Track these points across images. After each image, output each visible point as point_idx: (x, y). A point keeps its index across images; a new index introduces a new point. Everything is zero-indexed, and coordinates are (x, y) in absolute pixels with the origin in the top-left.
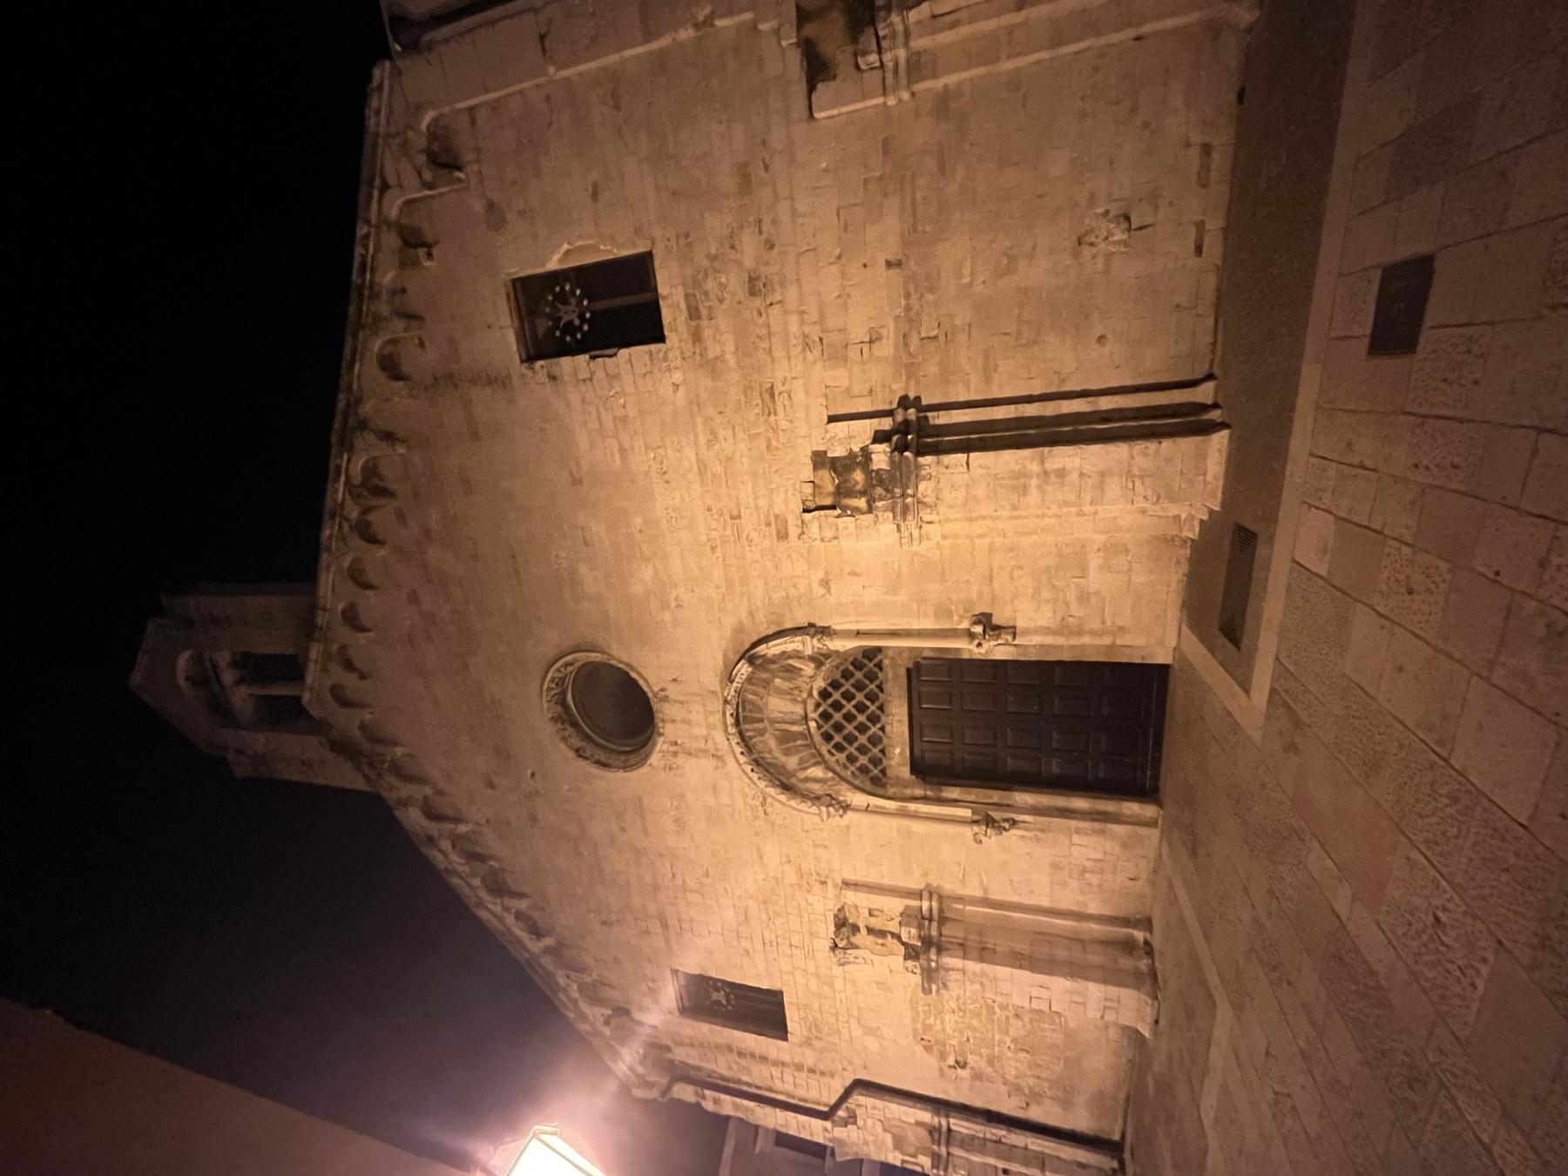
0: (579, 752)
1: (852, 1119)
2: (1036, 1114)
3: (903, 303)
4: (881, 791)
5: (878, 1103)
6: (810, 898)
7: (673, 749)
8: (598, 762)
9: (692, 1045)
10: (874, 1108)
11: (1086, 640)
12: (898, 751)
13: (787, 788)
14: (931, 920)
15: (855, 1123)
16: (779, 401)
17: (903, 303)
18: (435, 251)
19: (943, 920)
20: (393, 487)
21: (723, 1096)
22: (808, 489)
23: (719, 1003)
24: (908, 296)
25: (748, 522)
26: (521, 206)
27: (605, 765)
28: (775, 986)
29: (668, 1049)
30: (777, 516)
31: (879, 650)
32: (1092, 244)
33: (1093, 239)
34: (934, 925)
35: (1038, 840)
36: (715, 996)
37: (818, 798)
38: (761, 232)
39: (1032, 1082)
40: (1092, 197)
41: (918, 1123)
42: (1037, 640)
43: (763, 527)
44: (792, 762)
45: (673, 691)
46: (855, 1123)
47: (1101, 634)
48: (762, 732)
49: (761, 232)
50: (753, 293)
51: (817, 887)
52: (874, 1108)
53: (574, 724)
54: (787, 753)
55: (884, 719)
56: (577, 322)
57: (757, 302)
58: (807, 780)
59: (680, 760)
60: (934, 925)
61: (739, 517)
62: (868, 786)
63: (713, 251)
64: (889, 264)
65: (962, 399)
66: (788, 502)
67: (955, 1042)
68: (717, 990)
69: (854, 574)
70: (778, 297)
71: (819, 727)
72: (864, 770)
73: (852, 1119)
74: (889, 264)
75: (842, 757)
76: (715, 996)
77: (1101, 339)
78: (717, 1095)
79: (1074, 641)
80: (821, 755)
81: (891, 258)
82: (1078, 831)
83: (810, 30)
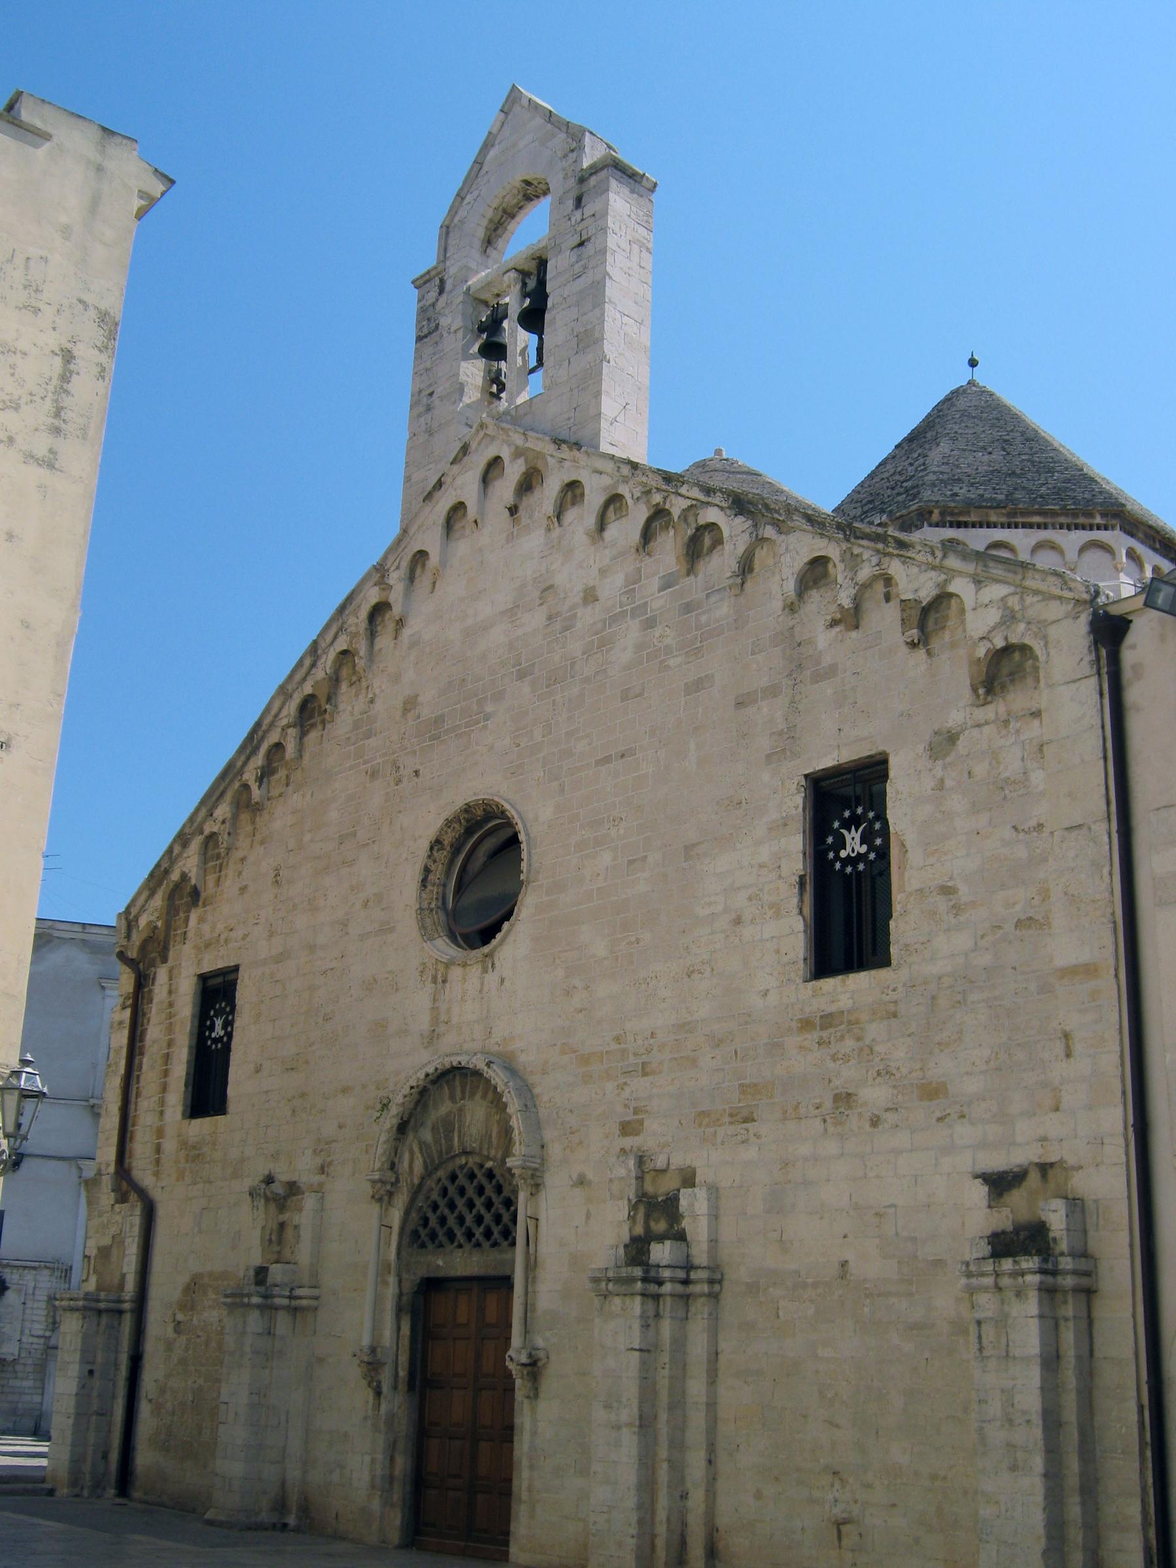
0: (437, 843)
1: (122, 1198)
2: (145, 1410)
3: (810, 1280)
4: (406, 1240)
5: (136, 1230)
6: (309, 1152)
7: (440, 979)
8: (427, 870)
9: (170, 992)
10: (132, 1225)
11: (525, 1474)
12: (440, 1263)
13: (402, 1128)
14: (290, 1298)
15: (117, 1202)
16: (739, 1128)
17: (810, 1280)
18: (921, 653)
19: (294, 1311)
20: (702, 567)
21: (126, 1033)
22: (660, 1163)
23: (212, 1028)
24: (815, 1285)
25: (640, 1085)
26: (949, 783)
27: (424, 882)
28: (232, 1106)
29: (165, 960)
30: (641, 1122)
31: (513, 1244)
32: (832, 1485)
33: (837, 1486)
34: (286, 1302)
35: (366, 1418)
36: (219, 1023)
37: (393, 1166)
38: (887, 1110)
39: (169, 1405)
40: (869, 1486)
41: (123, 1276)
42: (527, 1425)
43: (633, 1104)
44: (427, 1135)
45: (492, 978)
46: (117, 1202)
47: (530, 1490)
48: (452, 1098)
49: (887, 1110)
50: (837, 1098)
51: (319, 1161)
52: (132, 1225)
53: (469, 831)
54: (434, 1129)
55: (467, 1247)
56: (843, 854)
57: (828, 1104)
58: (412, 1153)
59: (430, 986)
60: (286, 1302)
61: (645, 1074)
62: (410, 1227)
63: (877, 1048)
64: (844, 1264)
65: (1134, 1368)
66: (655, 1135)
67: (195, 1321)
68: (224, 1027)
69: (588, 1216)
70: (831, 1129)
71: (462, 1167)
72: (425, 1222)
73: (122, 1198)
74: (844, 1264)
75: (435, 1196)
76: (219, 1023)
77: (758, 1495)
78: (128, 1022)
79: (525, 1462)
80: (436, 1169)
81: (851, 1264)
82: (373, 1461)
83: (1034, 1177)
